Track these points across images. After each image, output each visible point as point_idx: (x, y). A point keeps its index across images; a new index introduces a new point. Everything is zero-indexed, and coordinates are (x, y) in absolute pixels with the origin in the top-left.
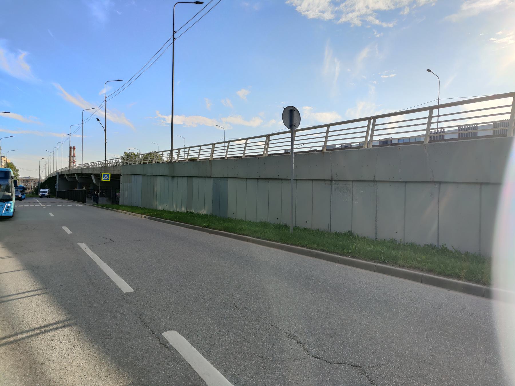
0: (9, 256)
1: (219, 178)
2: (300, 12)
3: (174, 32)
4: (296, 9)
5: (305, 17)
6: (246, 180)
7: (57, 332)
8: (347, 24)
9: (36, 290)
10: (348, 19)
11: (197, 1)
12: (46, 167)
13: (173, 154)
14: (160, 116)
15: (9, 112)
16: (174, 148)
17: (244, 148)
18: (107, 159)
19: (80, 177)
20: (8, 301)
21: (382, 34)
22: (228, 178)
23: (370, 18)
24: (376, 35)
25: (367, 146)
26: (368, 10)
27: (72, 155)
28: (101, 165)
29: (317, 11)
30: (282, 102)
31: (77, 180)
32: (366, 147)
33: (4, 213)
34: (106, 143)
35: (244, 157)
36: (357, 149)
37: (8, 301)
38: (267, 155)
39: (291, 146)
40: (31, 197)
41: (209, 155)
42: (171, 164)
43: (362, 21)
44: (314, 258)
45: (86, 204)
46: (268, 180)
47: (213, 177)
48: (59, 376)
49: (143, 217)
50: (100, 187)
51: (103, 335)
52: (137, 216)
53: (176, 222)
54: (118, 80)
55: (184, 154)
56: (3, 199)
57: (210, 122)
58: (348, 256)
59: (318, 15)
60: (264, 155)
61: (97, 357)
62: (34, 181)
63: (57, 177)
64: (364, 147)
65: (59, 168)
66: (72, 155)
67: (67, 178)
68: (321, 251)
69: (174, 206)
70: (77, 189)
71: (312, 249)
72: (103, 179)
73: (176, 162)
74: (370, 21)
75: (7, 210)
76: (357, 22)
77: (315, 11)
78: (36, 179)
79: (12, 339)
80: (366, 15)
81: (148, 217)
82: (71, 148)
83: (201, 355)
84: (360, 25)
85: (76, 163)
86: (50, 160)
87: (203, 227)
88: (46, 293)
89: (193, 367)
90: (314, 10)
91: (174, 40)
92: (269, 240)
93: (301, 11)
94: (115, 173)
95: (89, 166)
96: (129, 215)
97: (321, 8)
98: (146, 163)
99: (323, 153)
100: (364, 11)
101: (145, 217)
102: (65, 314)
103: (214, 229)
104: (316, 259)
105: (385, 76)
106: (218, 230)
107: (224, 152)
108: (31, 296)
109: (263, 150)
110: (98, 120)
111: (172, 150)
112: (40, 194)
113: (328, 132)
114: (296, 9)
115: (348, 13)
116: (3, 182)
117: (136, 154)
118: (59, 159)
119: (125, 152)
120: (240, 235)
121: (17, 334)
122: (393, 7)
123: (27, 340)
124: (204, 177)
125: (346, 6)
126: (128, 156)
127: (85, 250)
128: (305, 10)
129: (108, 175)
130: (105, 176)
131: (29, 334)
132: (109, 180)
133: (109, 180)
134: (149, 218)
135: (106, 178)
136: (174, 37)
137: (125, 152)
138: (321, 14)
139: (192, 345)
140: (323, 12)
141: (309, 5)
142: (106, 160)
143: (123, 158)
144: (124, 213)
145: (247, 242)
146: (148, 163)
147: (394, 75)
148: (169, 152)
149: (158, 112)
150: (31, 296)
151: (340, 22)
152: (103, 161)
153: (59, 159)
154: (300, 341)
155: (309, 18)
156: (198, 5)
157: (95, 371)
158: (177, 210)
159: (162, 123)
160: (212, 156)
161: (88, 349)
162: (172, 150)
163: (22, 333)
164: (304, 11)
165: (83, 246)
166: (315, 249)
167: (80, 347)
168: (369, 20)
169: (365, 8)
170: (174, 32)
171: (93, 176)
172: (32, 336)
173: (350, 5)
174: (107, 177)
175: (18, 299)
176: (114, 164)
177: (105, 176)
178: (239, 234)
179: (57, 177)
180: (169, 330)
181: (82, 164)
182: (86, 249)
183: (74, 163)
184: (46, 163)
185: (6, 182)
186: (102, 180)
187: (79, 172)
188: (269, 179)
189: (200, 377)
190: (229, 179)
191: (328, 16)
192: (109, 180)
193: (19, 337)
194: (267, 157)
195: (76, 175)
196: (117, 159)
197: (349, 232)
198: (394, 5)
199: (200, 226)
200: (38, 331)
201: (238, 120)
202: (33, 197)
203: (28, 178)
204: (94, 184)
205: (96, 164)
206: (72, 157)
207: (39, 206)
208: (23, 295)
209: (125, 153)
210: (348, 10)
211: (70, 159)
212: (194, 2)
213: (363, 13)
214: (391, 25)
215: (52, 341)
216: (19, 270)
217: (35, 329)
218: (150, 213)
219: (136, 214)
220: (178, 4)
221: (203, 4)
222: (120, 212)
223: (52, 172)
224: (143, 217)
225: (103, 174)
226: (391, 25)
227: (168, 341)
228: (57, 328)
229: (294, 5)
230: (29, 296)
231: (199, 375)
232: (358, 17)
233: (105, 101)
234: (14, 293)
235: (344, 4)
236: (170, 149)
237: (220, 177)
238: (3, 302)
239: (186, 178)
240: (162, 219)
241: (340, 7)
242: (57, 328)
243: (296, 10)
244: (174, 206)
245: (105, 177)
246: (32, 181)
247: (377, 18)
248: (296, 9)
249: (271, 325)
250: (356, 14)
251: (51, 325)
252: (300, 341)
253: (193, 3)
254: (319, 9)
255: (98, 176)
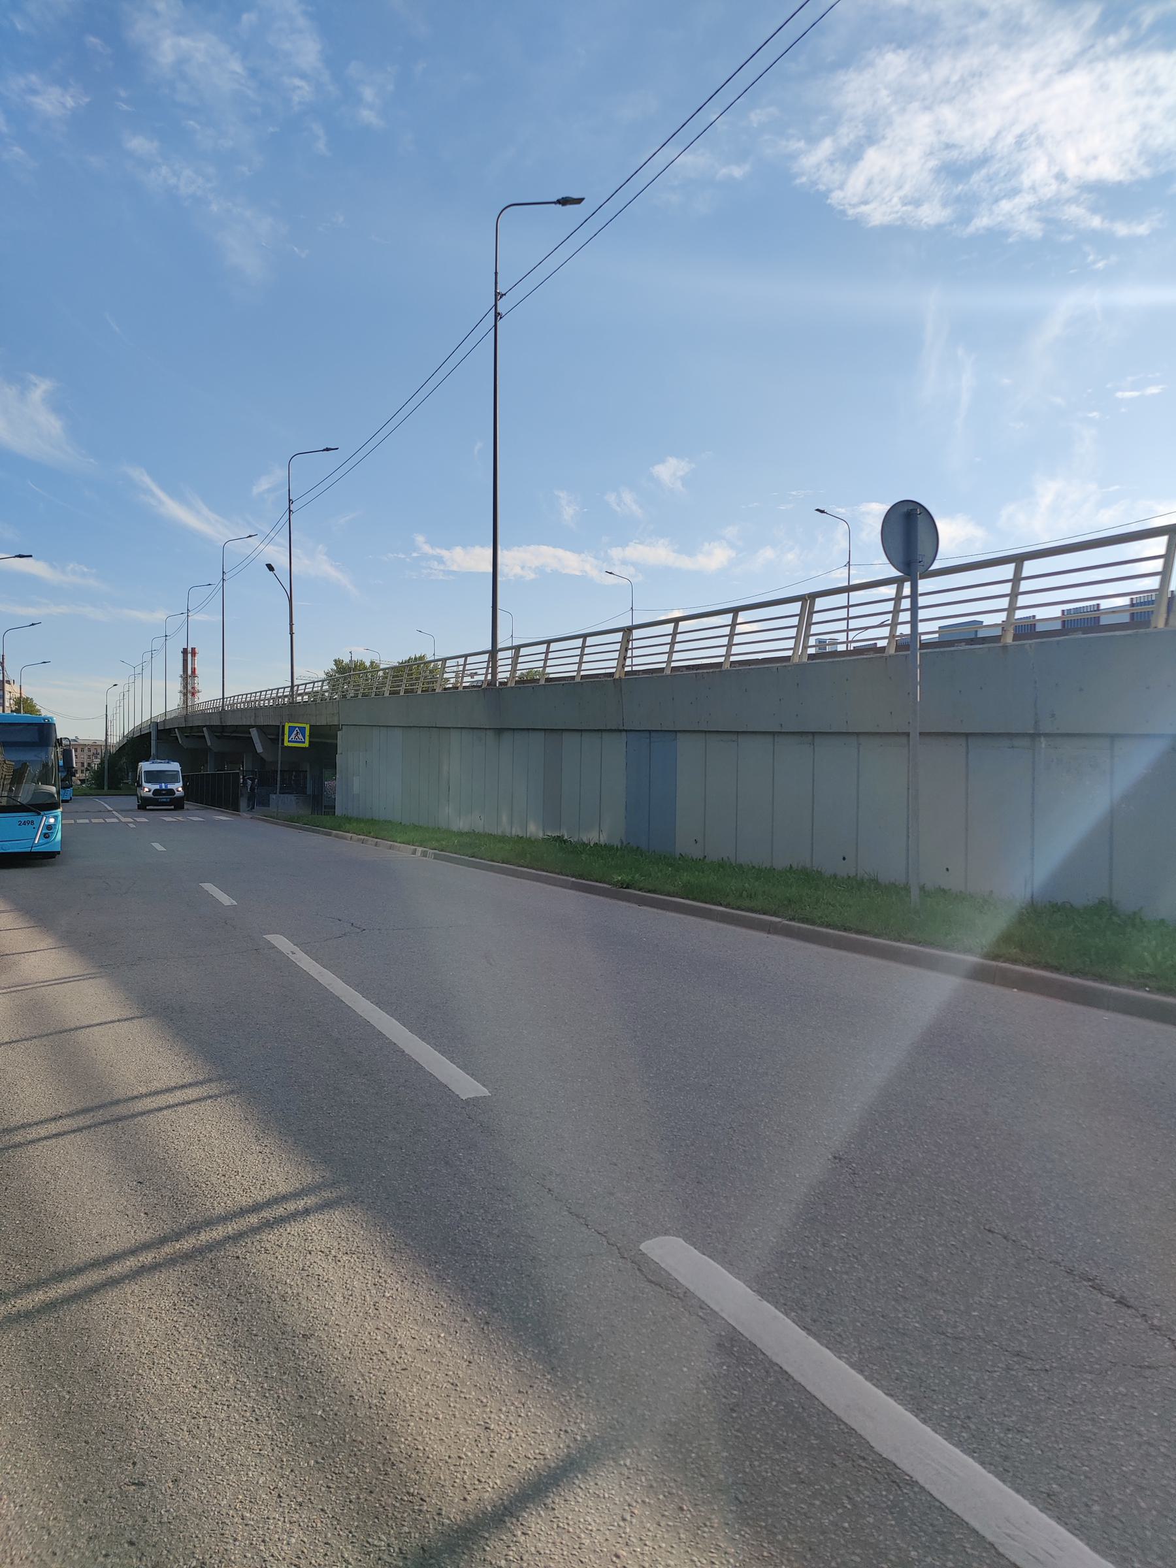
0: (86, 972)
1: (647, 735)
2: (842, 207)
3: (496, 294)
4: (828, 198)
5: (857, 223)
6: (734, 737)
7: (314, 1224)
8: (996, 236)
9: (201, 1083)
10: (1000, 218)
11: (564, 196)
12: (121, 708)
13: (500, 663)
14: (427, 549)
15: (31, 556)
16: (500, 646)
17: (727, 638)
18: (295, 683)
19: (216, 736)
20: (134, 1116)
21: (1114, 258)
22: (676, 732)
23: (1074, 212)
24: (1094, 262)
25: (1167, 620)
26: (1064, 187)
27: (189, 672)
28: (267, 702)
29: (895, 200)
30: (794, 493)
31: (209, 744)
32: (1161, 624)
33: (39, 845)
34: (292, 634)
35: (727, 666)
36: (1129, 632)
37: (134, 1116)
38: (805, 660)
39: (909, 625)
40: (86, 795)
41: (614, 663)
42: (491, 690)
43: (1046, 221)
44: (1015, 990)
45: (239, 815)
46: (811, 737)
47: (626, 731)
48: (372, 1382)
49: (419, 854)
50: (279, 765)
51: (454, 1240)
52: (399, 850)
53: (525, 869)
54: (324, 450)
55: (848, 607)
56: (34, 803)
57: (571, 562)
58: (1142, 987)
59: (899, 214)
60: (796, 660)
61: (468, 1319)
62: (89, 750)
63: (153, 737)
64: (1153, 625)
65: (158, 711)
66: (189, 672)
67: (179, 739)
68: (1035, 968)
69: (504, 819)
70: (210, 770)
71: (1005, 962)
72: (289, 741)
73: (509, 685)
74: (1071, 221)
75: (46, 836)
76: (1030, 227)
77: (890, 200)
78: (95, 745)
79: (186, 1244)
80: (1057, 202)
81: (435, 854)
82: (185, 652)
83: (804, 1333)
84: (1040, 234)
85: (197, 695)
86: (132, 690)
87: (614, 884)
88: (232, 1092)
89: (797, 1376)
90: (887, 199)
91: (499, 318)
92: (845, 930)
93: (843, 205)
94: (322, 721)
95: (234, 704)
96: (376, 845)
97: (907, 189)
98: (412, 691)
99: (1005, 647)
100: (1051, 189)
101: (424, 854)
102: (313, 1164)
103: (649, 891)
104: (1022, 994)
105: (1128, 394)
106: (665, 895)
107: (632, 657)
108: (193, 1101)
109: (791, 643)
110: (270, 568)
111: (493, 652)
112: (148, 789)
113: (1017, 579)
114: (829, 201)
115: (997, 200)
116: (36, 756)
117: (368, 664)
118: (159, 685)
119: (335, 661)
120: (742, 910)
121: (194, 1228)
122: (1146, 173)
123: (232, 1250)
124: (598, 730)
125: (989, 179)
126: (345, 672)
127: (290, 956)
128: (855, 200)
129: (303, 730)
130: (295, 732)
131: (231, 1228)
132: (306, 745)
133: (306, 745)
134: (436, 857)
135: (296, 738)
136: (499, 310)
137: (335, 661)
138: (909, 208)
139: (754, 1291)
140: (917, 203)
141: (870, 182)
142: (292, 687)
143: (330, 678)
144: (359, 840)
145: (769, 933)
146: (402, 693)
147: (1161, 387)
148: (486, 657)
149: (420, 539)
150: (193, 1101)
151: (971, 229)
152: (284, 688)
153: (159, 685)
154: (1122, 1297)
155: (870, 225)
156: (569, 207)
157: (480, 1368)
158: (514, 833)
159: (436, 570)
160: (623, 666)
161: (430, 1290)
162: (493, 652)
163: (209, 1223)
164: (854, 206)
165: (281, 942)
166: (1014, 961)
167: (402, 1281)
168: (1066, 217)
169: (1053, 181)
170: (498, 296)
171: (254, 733)
172: (241, 1235)
173: (1002, 174)
174: (300, 736)
175: (160, 1109)
176: (307, 697)
177: (295, 732)
178: (739, 908)
179: (153, 737)
180: (657, 1234)
181: (223, 698)
182: (293, 953)
183: (193, 694)
184: (122, 698)
185: (43, 756)
186: (286, 744)
187: (216, 722)
188: (813, 734)
189: (839, 1420)
190: (679, 735)
191: (931, 214)
192: (304, 742)
193: (205, 1237)
194: (804, 664)
195: (205, 729)
196: (317, 682)
197: (1102, 902)
198: (1148, 164)
199: (605, 882)
200: (254, 1219)
201: (658, 553)
202: (91, 795)
203: (75, 740)
204: (258, 754)
205: (257, 698)
206: (188, 676)
207: (115, 820)
208: (170, 1099)
209: (337, 662)
210: (996, 189)
211: (185, 686)
212: (555, 200)
213: (1049, 196)
214: (1142, 229)
215: (309, 1256)
216: (132, 1018)
217: (243, 1212)
218: (438, 841)
219: (396, 844)
220: (511, 207)
221: (584, 202)
222: (346, 839)
223: (138, 723)
224: (419, 854)
225: (287, 726)
226: (1142, 229)
227: (670, 1275)
228: (307, 1212)
229: (822, 187)
230: (189, 1103)
231: (831, 1411)
232: (1030, 209)
233: (290, 511)
234: (143, 1090)
235: (984, 172)
236: (489, 647)
237: (650, 731)
238: (120, 1119)
239: (542, 733)
240: (478, 860)
241: (972, 181)
242: (307, 1212)
243: (830, 205)
244: (504, 819)
245: (293, 736)
246: (82, 750)
247: (1094, 210)
248: (829, 201)
249: (989, 1231)
250: (1028, 199)
251: (285, 1198)
252: (1122, 1297)
253: (553, 205)
254: (902, 193)
255: (273, 734)
